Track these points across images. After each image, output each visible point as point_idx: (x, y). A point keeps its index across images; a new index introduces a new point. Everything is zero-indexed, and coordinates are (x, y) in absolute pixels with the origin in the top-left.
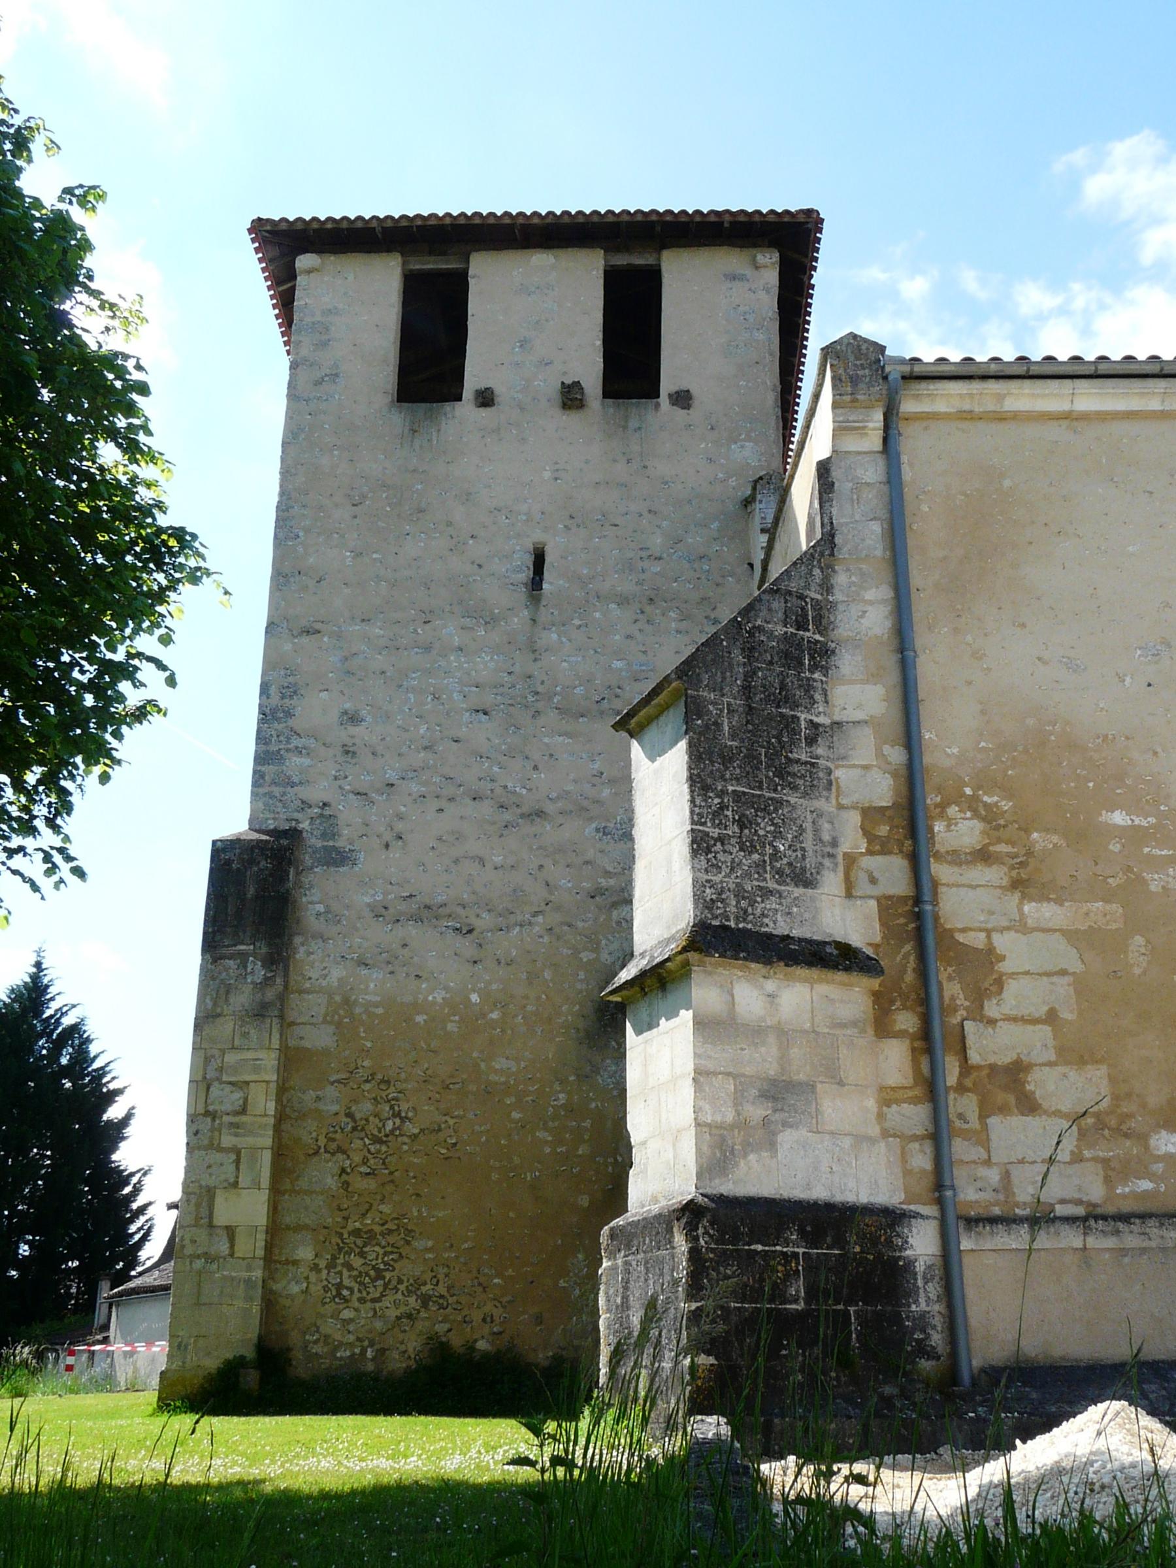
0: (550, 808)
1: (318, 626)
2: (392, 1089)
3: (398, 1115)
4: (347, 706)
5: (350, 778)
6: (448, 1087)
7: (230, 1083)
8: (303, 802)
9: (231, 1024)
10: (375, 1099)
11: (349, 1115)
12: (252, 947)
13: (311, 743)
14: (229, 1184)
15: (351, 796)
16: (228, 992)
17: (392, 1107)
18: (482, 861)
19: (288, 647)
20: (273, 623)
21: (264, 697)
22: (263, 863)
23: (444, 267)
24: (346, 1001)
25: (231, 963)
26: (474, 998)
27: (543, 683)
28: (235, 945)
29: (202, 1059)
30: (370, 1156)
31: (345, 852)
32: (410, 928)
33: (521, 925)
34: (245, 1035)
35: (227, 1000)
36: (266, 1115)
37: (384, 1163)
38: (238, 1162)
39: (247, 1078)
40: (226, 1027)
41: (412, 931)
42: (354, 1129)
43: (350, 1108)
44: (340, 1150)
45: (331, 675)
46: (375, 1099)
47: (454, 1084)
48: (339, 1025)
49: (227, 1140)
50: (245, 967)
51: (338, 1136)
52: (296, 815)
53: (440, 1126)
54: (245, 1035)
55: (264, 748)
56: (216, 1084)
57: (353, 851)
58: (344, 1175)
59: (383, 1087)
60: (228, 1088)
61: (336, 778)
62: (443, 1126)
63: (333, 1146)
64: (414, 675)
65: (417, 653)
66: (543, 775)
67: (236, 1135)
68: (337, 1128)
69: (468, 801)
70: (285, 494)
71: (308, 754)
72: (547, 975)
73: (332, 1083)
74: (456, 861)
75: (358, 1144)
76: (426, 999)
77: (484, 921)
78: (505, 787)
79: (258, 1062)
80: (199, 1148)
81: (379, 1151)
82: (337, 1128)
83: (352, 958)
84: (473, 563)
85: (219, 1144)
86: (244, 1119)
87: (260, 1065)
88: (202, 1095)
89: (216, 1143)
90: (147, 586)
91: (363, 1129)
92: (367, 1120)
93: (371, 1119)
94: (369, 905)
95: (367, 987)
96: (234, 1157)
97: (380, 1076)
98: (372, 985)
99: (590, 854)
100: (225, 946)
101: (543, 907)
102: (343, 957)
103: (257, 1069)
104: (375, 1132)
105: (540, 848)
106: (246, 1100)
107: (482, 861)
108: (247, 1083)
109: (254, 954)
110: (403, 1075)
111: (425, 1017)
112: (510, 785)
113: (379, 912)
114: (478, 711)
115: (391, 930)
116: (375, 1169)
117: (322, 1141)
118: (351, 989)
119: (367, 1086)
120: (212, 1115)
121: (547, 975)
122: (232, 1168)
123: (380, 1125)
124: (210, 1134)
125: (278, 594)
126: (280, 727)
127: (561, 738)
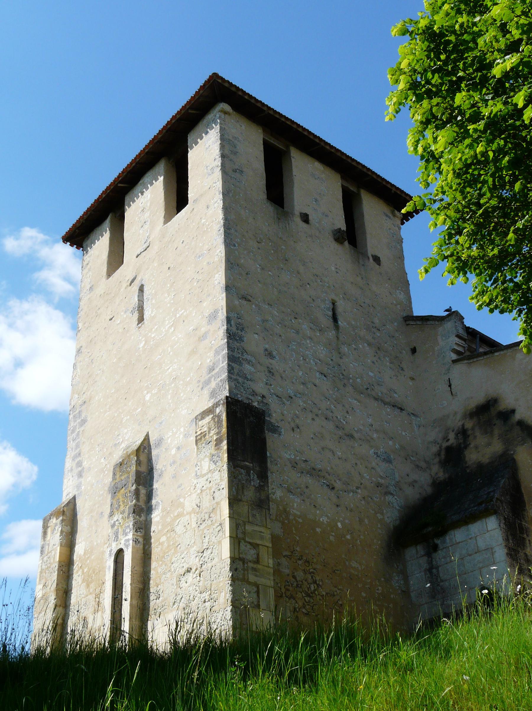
0: (355, 435)
1: (249, 298)
2: (311, 567)
3: (315, 582)
4: (267, 346)
5: (273, 386)
6: (334, 572)
7: (250, 543)
8: (253, 391)
9: (247, 507)
10: (304, 570)
11: (294, 577)
12: (252, 465)
13: (253, 359)
14: (255, 605)
15: (275, 396)
16: (243, 488)
17: (312, 577)
18: (333, 453)
19: (237, 302)
20: (228, 286)
21: (229, 325)
22: (252, 418)
23: (277, 145)
24: (285, 510)
25: (242, 471)
26: (339, 525)
27: (344, 371)
28: (244, 461)
29: (235, 524)
30: (306, 604)
31: (275, 426)
32: (308, 478)
33: (353, 492)
34: (254, 516)
35: (243, 493)
36: (269, 567)
37: (312, 609)
38: (258, 592)
39: (259, 542)
40: (244, 509)
41: (309, 480)
42: (297, 585)
43: (294, 573)
44: (291, 597)
45: (258, 327)
46: (304, 570)
47: (337, 570)
48: (283, 523)
49: (252, 578)
50: (249, 476)
51: (291, 588)
52: (250, 397)
53: (334, 593)
54: (254, 516)
55: (231, 353)
56: (242, 541)
57: (279, 427)
58: (296, 613)
59: (307, 564)
60: (249, 546)
61: (267, 384)
62: (335, 593)
63: (288, 593)
64: (293, 343)
65: (293, 332)
66: (351, 418)
67: (256, 576)
68: (289, 583)
69: (323, 418)
70: (226, 219)
71: (253, 365)
72: (366, 521)
73: (284, 556)
74: (323, 449)
75: (299, 595)
76: (319, 520)
77: (338, 485)
78: (337, 417)
79: (262, 534)
80: (238, 579)
81: (309, 602)
82: (289, 583)
83: (285, 487)
84: (310, 297)
85: (248, 579)
86: (259, 567)
87: (263, 536)
88: (237, 547)
89: (246, 578)
90: (518, 219)
91: (301, 587)
92: (302, 582)
93: (304, 581)
94: (289, 459)
95: (293, 505)
96: (255, 589)
97: (305, 558)
98: (295, 504)
99: (374, 464)
100: (239, 460)
101: (359, 485)
102: (280, 485)
103: (262, 538)
104: (306, 590)
105: (354, 454)
106: (258, 555)
107: (333, 453)
108: (258, 545)
109: (253, 470)
110: (315, 560)
111: (320, 530)
112: (339, 417)
113: (294, 465)
114: (322, 374)
115: (300, 477)
116: (309, 612)
117: (283, 590)
118: (287, 504)
119: (300, 562)
120: (243, 560)
121: (366, 521)
122: (255, 596)
123: (308, 586)
124: (242, 572)
125: (229, 271)
126: (238, 344)
127: (356, 401)
